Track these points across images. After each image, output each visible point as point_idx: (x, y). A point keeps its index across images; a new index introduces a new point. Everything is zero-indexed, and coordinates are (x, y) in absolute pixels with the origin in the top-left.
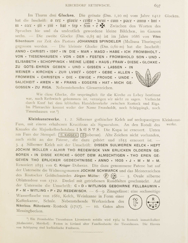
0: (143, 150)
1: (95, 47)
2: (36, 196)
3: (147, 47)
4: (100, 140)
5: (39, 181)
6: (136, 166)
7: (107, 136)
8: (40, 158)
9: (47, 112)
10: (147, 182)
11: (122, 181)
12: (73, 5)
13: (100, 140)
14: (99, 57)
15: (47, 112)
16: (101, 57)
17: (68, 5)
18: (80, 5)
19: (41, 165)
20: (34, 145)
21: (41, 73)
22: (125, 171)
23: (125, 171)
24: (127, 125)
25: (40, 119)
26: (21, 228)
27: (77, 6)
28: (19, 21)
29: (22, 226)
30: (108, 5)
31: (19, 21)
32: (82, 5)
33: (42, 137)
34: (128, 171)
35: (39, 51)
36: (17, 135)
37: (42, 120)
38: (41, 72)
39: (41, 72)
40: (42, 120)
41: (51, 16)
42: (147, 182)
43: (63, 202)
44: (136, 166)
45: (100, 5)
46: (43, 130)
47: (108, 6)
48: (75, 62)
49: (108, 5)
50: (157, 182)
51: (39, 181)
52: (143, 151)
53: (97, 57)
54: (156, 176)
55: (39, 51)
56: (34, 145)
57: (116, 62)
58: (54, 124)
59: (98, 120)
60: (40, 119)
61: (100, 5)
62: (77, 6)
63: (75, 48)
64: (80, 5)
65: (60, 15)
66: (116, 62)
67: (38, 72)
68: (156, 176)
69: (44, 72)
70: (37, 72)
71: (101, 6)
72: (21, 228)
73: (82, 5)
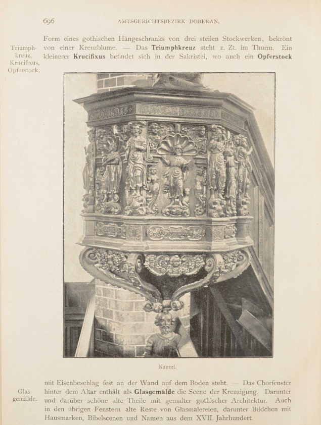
2: (103, 39)
4: (99, 401)
5: (158, 411)
7: (234, 402)
10: (257, 401)
11: (120, 401)
13: (99, 401)
18: (196, 21)
22: (53, 401)
23: (53, 401)
24: (237, 401)
33: (154, 406)
34: (62, 401)
37: (165, 48)
40: (165, 48)
41: (186, 39)
42: (257, 401)
50: (280, 401)
51: (158, 411)
54: (116, 410)
56: (77, 401)
58: (185, 401)
59: (202, 401)
63: (74, 394)
64: (196, 21)
65: (137, 391)
68: (116, 410)
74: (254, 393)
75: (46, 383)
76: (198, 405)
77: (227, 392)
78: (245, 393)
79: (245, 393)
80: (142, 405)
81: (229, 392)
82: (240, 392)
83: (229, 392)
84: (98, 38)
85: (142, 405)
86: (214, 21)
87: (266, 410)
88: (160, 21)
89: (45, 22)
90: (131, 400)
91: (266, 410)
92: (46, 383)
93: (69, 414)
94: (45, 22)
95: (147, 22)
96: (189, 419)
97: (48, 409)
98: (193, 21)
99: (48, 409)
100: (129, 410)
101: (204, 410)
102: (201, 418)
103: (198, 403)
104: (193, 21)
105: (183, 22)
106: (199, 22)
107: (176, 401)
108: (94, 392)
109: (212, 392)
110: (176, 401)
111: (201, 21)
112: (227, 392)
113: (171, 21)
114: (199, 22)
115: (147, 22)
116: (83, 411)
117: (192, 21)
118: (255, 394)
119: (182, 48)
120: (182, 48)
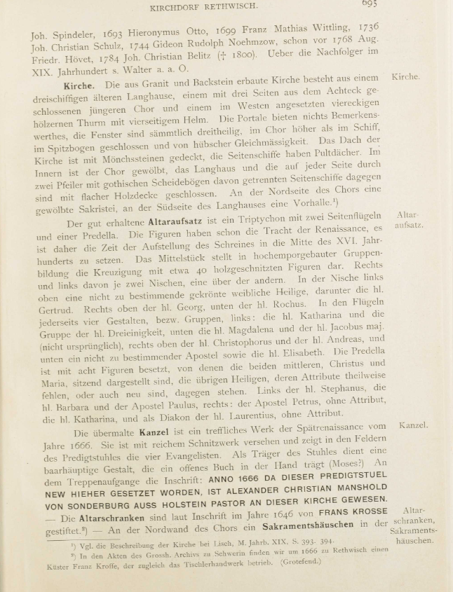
0: (308, 476)
1: (295, 143)
3: (171, 482)
10: (199, 158)
12: (168, 8)
14: (191, 504)
16: (193, 491)
17: (155, 8)
21: (316, 502)
24: (334, 341)
27: (177, 8)
30: (252, 5)
32: (190, 7)
35: (306, 489)
38: (315, 500)
39: (315, 500)
42: (199, 158)
43: (232, 44)
45: (232, 6)
46: (236, 331)
47: (252, 7)
48: (197, 505)
49: (252, 5)
52: (308, 478)
53: (187, 504)
55: (306, 489)
57: (327, 512)
61: (232, 6)
62: (177, 8)
64: (186, 7)
66: (327, 512)
67: (309, 501)
69: (322, 501)
70: (306, 501)
71: (236, 7)
73: (190, 7)
74: (236, 132)
77: (101, 274)
78: (302, 269)
79: (302, 269)
80: (321, 46)
81: (104, 273)
82: (118, 273)
83: (104, 273)
84: (298, 27)
87: (259, 294)
90: (83, 123)
91: (259, 294)
96: (316, 92)
102: (343, 241)
107: (256, 43)
108: (201, 133)
110: (256, 43)
112: (279, 81)
118: (345, 30)
119: (279, 527)
120: (279, 527)
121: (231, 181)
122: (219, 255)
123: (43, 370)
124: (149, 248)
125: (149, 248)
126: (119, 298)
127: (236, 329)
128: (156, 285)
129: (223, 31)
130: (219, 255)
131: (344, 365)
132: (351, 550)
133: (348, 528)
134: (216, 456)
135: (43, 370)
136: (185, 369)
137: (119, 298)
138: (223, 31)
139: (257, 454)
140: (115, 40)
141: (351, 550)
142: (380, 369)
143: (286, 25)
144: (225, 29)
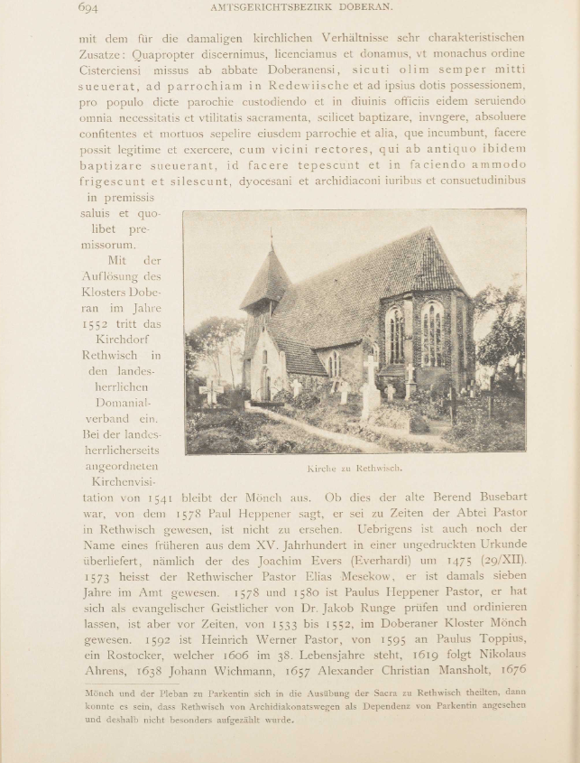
6: (215, 514)
8: (253, 647)
9: (204, 672)
15: (204, 672)
18: (350, 7)
19: (337, 624)
20: (291, 71)
25: (501, 545)
26: (428, 707)
28: (523, 592)
29: (432, 700)
31: (523, 592)
32: (222, 7)
36: (134, 436)
44: (215, 514)
46: (449, 671)
54: (232, 55)
56: (291, 71)
60: (501, 545)
64: (350, 7)
68: (232, 55)
72: (428, 707)
73: (222, 7)
75: (82, 40)
76: (173, 602)
77: (105, 340)
85: (145, 584)
86: (382, 6)
87: (415, 102)
88: (233, 7)
89: (82, 8)
92: (82, 40)
93: (474, 174)
94: (82, 8)
95: (265, 7)
97: (89, 531)
98: (347, 7)
99: (89, 531)
100: (381, 134)
101: (451, 498)
103: (174, 597)
104: (347, 7)
105: (328, 7)
106: (356, 7)
109: (363, 55)
111: (361, 6)
113: (307, 7)
114: (356, 7)
115: (265, 7)
116: (393, 532)
117: (343, 7)
121: (255, 625)
122: (383, 653)
123: (328, 590)
124: (91, 277)
125: (91, 277)
126: (283, 531)
127: (449, 668)
128: (488, 655)
129: (232, 656)
130: (383, 653)
131: (401, 672)
132: (379, 469)
133: (299, 12)
134: (214, 593)
135: (328, 590)
136: (361, 640)
137: (283, 531)
138: (232, 656)
139: (486, 639)
140: (390, 648)
141: (379, 469)
142: (86, 95)
143: (426, 689)
144: (235, 653)
